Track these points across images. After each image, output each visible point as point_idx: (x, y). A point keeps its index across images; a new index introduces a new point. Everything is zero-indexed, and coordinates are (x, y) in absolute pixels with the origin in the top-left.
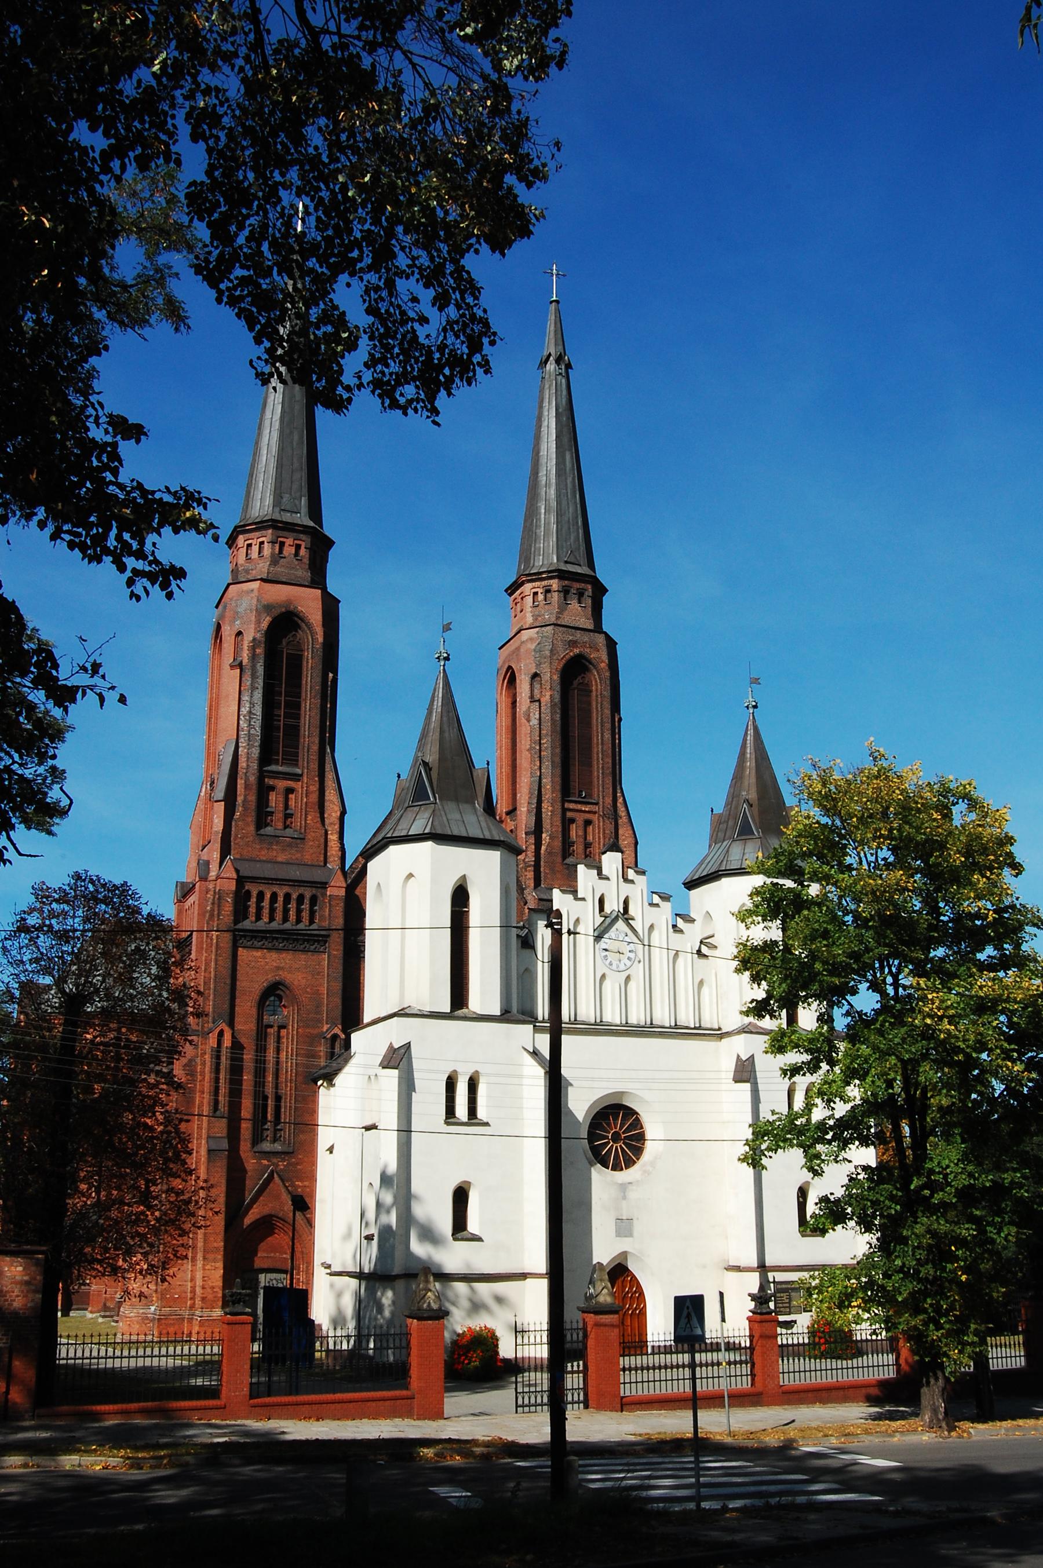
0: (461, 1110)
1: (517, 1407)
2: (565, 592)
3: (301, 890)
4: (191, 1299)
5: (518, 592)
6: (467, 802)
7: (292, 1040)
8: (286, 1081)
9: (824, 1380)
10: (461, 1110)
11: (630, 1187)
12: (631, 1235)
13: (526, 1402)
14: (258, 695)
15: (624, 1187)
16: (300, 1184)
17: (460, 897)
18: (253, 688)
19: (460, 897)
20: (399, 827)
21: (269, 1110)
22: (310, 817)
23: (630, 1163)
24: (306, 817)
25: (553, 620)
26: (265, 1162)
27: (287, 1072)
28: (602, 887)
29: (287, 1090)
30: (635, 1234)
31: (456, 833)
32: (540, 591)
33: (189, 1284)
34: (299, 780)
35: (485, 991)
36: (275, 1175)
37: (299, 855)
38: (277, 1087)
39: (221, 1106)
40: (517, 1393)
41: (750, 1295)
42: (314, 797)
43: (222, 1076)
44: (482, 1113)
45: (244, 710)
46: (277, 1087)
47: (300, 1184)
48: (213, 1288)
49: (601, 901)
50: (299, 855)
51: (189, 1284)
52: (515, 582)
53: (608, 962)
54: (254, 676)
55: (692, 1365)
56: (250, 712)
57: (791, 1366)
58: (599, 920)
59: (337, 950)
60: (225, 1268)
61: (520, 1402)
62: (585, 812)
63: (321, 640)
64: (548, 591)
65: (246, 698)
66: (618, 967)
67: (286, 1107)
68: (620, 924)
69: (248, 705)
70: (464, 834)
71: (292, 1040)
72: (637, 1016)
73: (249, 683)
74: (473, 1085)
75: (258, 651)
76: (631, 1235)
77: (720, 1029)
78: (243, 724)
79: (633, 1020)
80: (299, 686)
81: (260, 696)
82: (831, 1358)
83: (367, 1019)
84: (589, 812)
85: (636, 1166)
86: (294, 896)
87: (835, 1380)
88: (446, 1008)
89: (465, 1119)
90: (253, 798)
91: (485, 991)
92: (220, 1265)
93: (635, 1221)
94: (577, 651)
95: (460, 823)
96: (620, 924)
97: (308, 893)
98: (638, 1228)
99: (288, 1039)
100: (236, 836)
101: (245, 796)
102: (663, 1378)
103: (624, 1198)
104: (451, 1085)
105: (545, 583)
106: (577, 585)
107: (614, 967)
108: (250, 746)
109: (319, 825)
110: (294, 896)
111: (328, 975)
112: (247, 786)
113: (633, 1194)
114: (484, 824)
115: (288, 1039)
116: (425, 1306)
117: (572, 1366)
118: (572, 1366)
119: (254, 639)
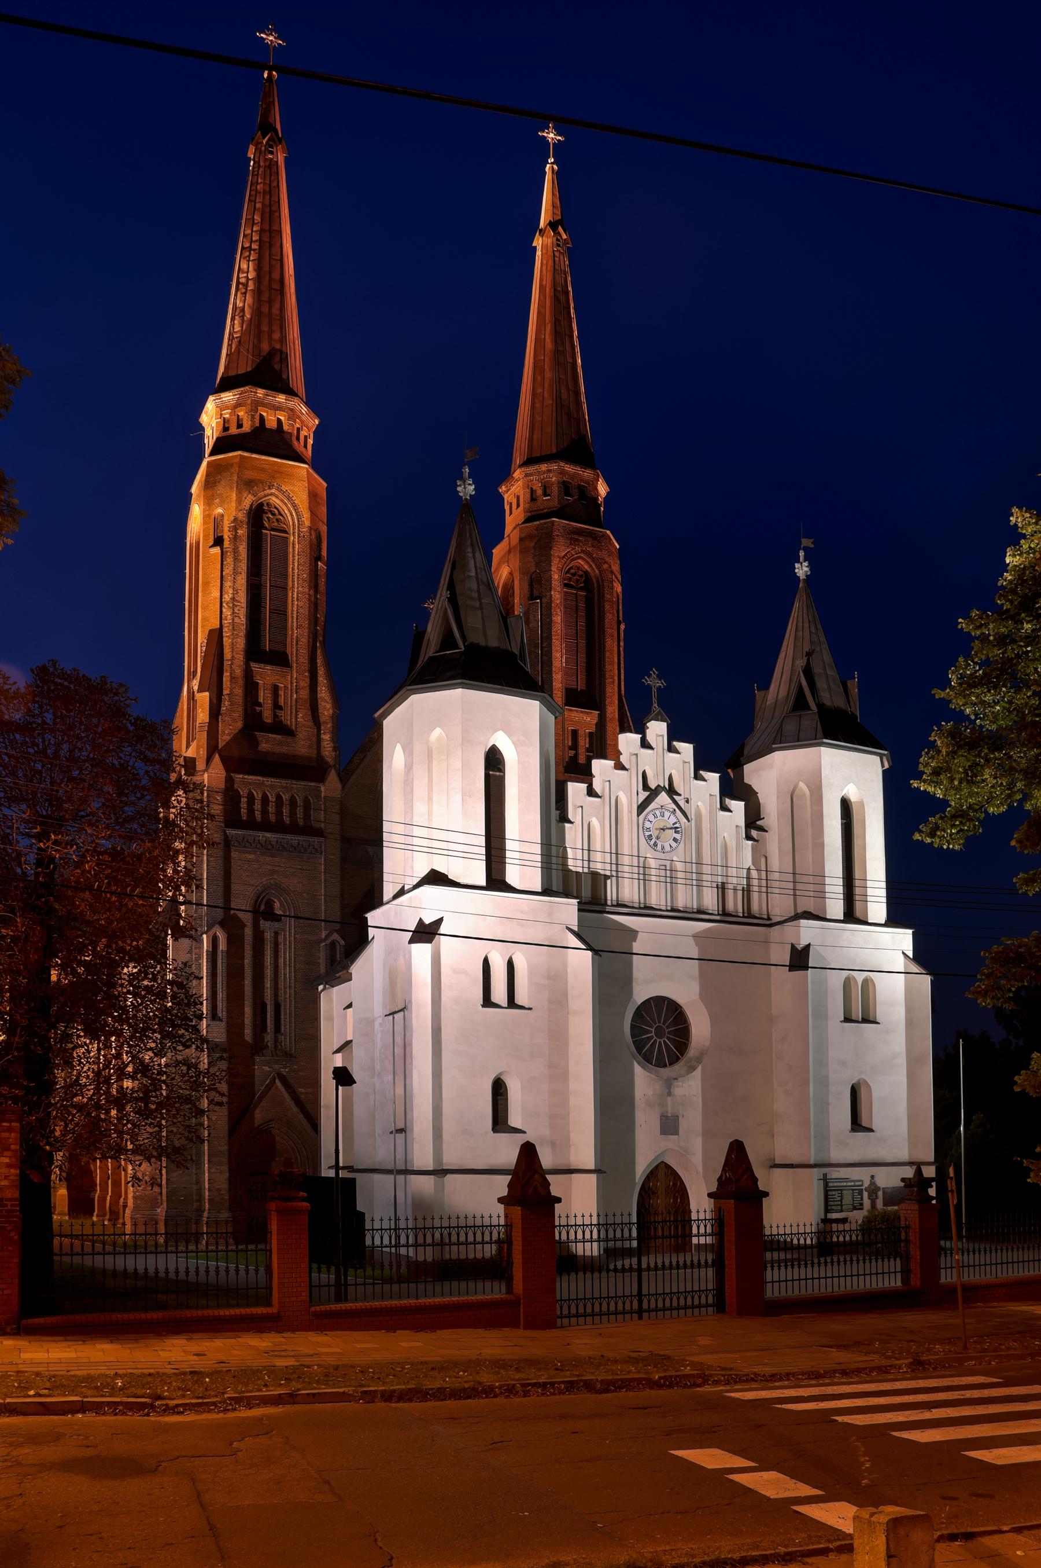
0: (499, 994)
4: (197, 1201)
7: (290, 947)
8: (285, 988)
9: (971, 1277)
10: (499, 994)
12: (677, 1133)
13: (581, 1311)
14: (242, 580)
16: (303, 1090)
18: (235, 573)
21: (268, 1022)
24: (296, 715)
26: (266, 1068)
27: (285, 978)
29: (286, 996)
30: (681, 1132)
33: (195, 1187)
35: (523, 868)
36: (277, 1081)
38: (276, 995)
39: (219, 1010)
42: (305, 693)
43: (219, 979)
44: (520, 998)
45: (227, 598)
46: (276, 995)
47: (303, 1090)
48: (219, 1190)
51: (195, 1187)
54: (236, 559)
56: (233, 599)
57: (988, 1259)
60: (230, 1171)
63: (307, 523)
65: (228, 584)
66: (655, 844)
67: (285, 1014)
68: (663, 798)
69: (231, 591)
71: (290, 947)
73: (231, 568)
75: (240, 532)
76: (677, 1133)
77: (769, 919)
78: (227, 612)
79: (680, 904)
81: (244, 582)
83: (386, 898)
87: (829, 1289)
88: (484, 883)
89: (505, 1004)
90: (239, 691)
91: (523, 868)
92: (225, 1168)
93: (680, 1118)
96: (663, 798)
99: (285, 945)
100: (223, 732)
101: (231, 690)
102: (783, 1278)
103: (670, 1094)
107: (659, 848)
108: (234, 636)
109: (311, 724)
111: (325, 881)
112: (232, 678)
115: (285, 945)
117: (851, 1236)
118: (851, 1236)
119: (235, 520)
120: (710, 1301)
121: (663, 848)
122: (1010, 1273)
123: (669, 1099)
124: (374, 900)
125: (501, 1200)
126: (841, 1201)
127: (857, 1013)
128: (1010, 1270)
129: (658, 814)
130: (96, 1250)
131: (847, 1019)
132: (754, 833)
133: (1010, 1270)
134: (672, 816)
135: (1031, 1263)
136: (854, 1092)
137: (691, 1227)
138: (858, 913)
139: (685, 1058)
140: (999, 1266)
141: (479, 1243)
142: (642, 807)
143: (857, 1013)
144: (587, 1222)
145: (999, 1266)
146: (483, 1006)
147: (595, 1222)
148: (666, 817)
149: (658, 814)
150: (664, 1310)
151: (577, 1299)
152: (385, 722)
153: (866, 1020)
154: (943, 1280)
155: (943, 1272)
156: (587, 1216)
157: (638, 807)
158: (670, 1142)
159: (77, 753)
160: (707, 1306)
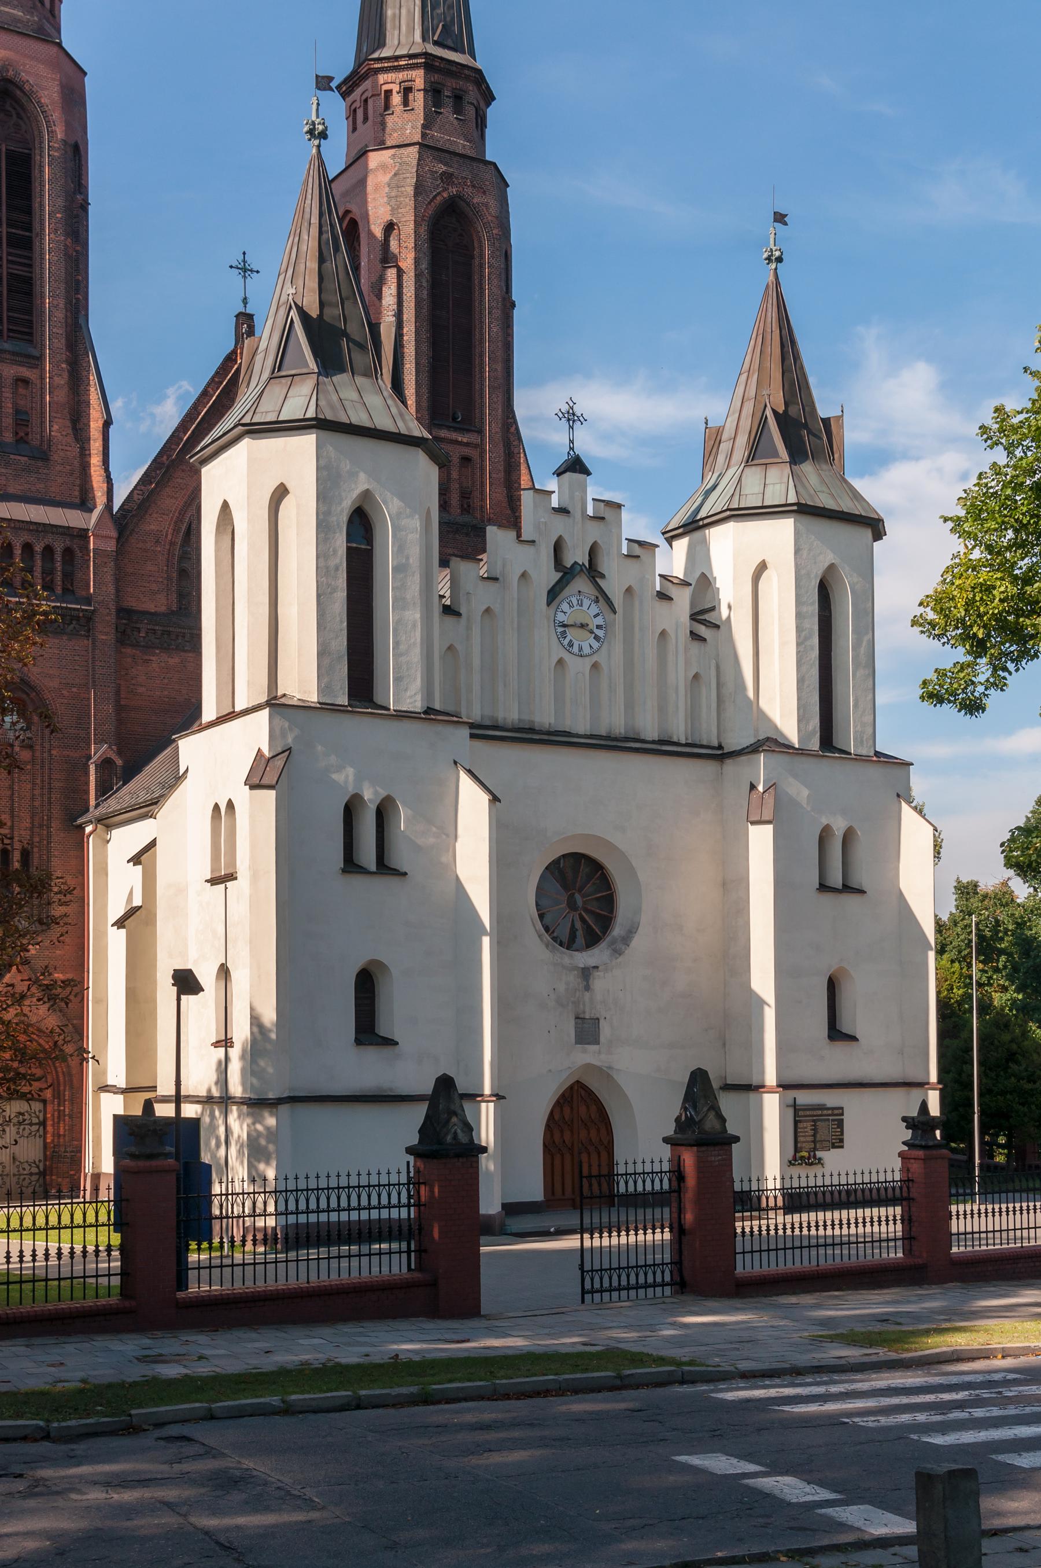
0: (367, 855)
1: (584, 1292)
2: (434, 92)
3: (49, 540)
5: (359, 91)
6: (366, 374)
10: (367, 855)
11: (596, 974)
12: (597, 1042)
15: (586, 973)
17: (362, 524)
19: (362, 524)
20: (260, 409)
22: (56, 427)
23: (593, 940)
25: (417, 138)
28: (559, 527)
30: (602, 1039)
31: (355, 420)
32: (395, 88)
34: (35, 366)
37: (41, 486)
40: (583, 1272)
41: (904, 1119)
49: (558, 547)
50: (41, 486)
52: (354, 72)
53: (566, 642)
55: (1008, 1230)
58: (557, 576)
59: (107, 634)
61: (588, 1286)
62: (461, 443)
64: (407, 91)
66: (581, 649)
68: (581, 584)
70: (368, 424)
72: (614, 721)
74: (384, 813)
76: (597, 1042)
77: (720, 747)
80: (29, 211)
82: (644, 1194)
84: (467, 444)
85: (603, 945)
86: (38, 548)
89: (373, 867)
93: (602, 1021)
94: (454, 191)
95: (359, 406)
96: (581, 584)
97: (59, 547)
98: (605, 1031)
103: (587, 988)
104: (350, 811)
105: (401, 76)
106: (451, 83)
107: (575, 649)
109: (70, 439)
110: (38, 548)
113: (600, 983)
114: (394, 410)
116: (449, 1138)
120: (667, 1278)
121: (581, 649)
122: (789, 1264)
123: (587, 994)
124: (186, 716)
125: (409, 1150)
126: (814, 1135)
127: (836, 879)
128: (781, 1260)
129: (575, 602)
130: (38, 1225)
131: (824, 887)
132: (702, 630)
133: (781, 1260)
134: (593, 605)
135: (789, 1252)
136: (832, 986)
137: (211, 1202)
138: (838, 743)
139: (608, 939)
140: (756, 1255)
141: (292, 1213)
142: (553, 594)
143: (836, 879)
144: (394, 1179)
145: (781, 1253)
146: (344, 871)
147: (404, 1179)
148: (585, 607)
149: (575, 602)
150: (610, 1291)
151: (610, 1269)
152: (205, 471)
153: (847, 888)
154: (739, 1269)
155: (739, 1257)
156: (394, 1171)
157: (549, 592)
158: (587, 1056)
159: (1004, 901)
160: (663, 1285)
